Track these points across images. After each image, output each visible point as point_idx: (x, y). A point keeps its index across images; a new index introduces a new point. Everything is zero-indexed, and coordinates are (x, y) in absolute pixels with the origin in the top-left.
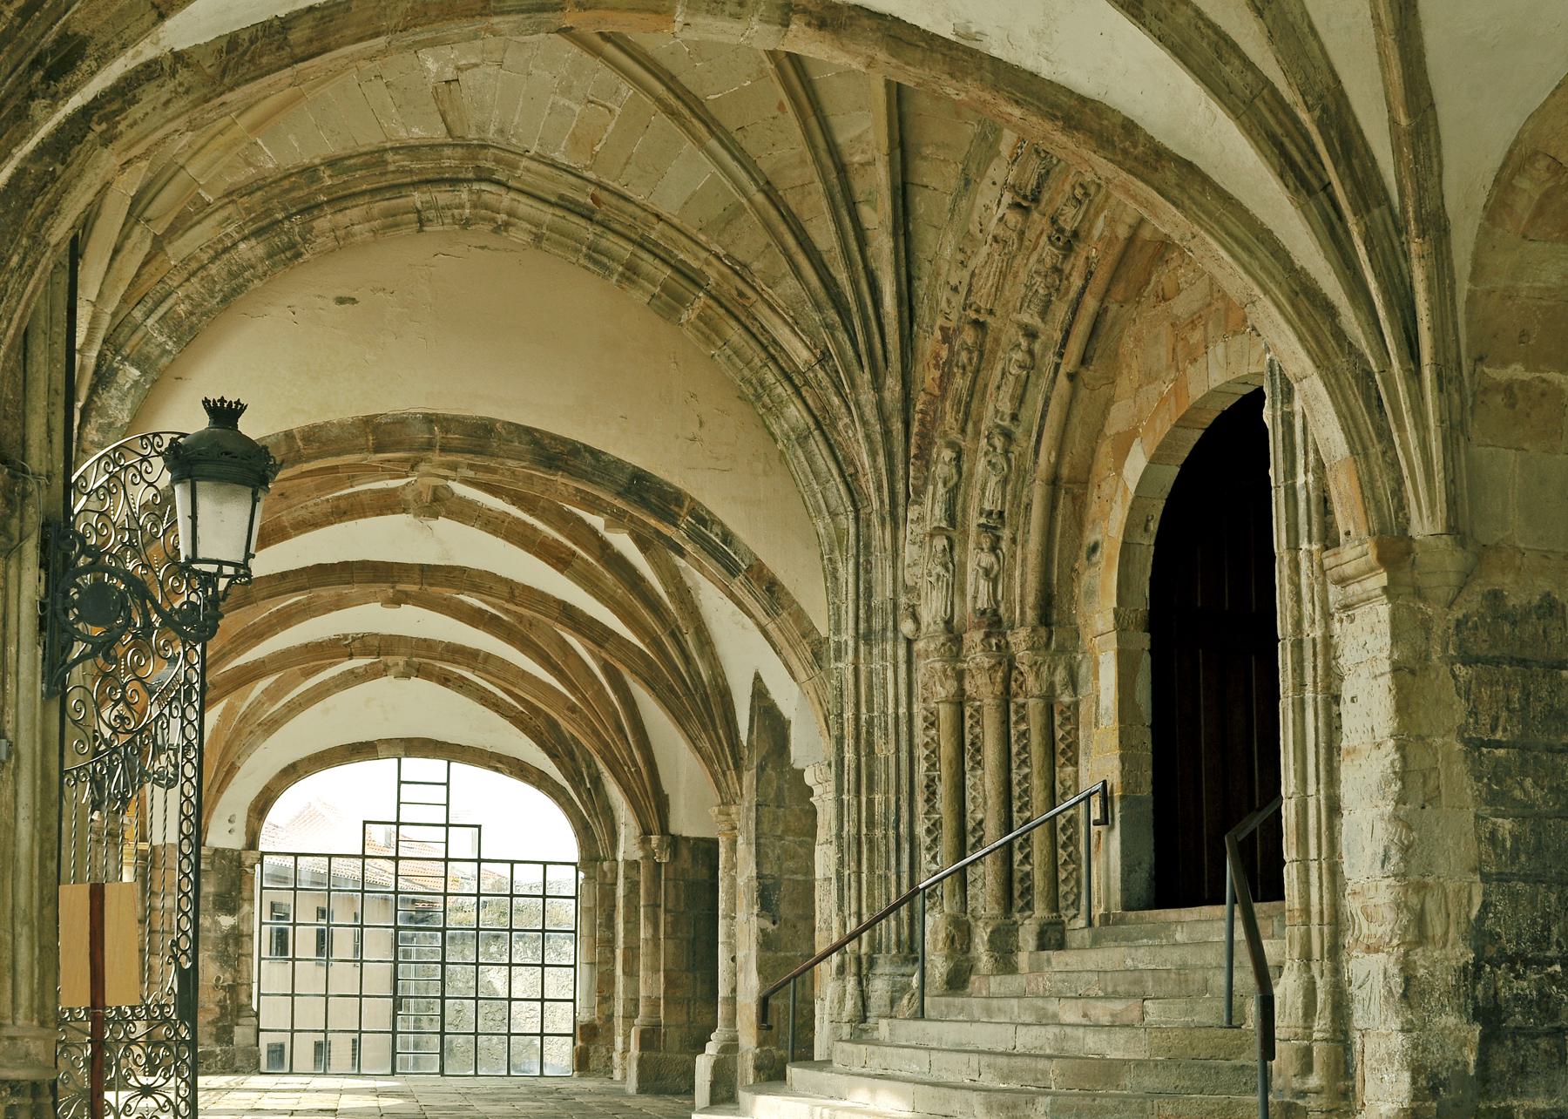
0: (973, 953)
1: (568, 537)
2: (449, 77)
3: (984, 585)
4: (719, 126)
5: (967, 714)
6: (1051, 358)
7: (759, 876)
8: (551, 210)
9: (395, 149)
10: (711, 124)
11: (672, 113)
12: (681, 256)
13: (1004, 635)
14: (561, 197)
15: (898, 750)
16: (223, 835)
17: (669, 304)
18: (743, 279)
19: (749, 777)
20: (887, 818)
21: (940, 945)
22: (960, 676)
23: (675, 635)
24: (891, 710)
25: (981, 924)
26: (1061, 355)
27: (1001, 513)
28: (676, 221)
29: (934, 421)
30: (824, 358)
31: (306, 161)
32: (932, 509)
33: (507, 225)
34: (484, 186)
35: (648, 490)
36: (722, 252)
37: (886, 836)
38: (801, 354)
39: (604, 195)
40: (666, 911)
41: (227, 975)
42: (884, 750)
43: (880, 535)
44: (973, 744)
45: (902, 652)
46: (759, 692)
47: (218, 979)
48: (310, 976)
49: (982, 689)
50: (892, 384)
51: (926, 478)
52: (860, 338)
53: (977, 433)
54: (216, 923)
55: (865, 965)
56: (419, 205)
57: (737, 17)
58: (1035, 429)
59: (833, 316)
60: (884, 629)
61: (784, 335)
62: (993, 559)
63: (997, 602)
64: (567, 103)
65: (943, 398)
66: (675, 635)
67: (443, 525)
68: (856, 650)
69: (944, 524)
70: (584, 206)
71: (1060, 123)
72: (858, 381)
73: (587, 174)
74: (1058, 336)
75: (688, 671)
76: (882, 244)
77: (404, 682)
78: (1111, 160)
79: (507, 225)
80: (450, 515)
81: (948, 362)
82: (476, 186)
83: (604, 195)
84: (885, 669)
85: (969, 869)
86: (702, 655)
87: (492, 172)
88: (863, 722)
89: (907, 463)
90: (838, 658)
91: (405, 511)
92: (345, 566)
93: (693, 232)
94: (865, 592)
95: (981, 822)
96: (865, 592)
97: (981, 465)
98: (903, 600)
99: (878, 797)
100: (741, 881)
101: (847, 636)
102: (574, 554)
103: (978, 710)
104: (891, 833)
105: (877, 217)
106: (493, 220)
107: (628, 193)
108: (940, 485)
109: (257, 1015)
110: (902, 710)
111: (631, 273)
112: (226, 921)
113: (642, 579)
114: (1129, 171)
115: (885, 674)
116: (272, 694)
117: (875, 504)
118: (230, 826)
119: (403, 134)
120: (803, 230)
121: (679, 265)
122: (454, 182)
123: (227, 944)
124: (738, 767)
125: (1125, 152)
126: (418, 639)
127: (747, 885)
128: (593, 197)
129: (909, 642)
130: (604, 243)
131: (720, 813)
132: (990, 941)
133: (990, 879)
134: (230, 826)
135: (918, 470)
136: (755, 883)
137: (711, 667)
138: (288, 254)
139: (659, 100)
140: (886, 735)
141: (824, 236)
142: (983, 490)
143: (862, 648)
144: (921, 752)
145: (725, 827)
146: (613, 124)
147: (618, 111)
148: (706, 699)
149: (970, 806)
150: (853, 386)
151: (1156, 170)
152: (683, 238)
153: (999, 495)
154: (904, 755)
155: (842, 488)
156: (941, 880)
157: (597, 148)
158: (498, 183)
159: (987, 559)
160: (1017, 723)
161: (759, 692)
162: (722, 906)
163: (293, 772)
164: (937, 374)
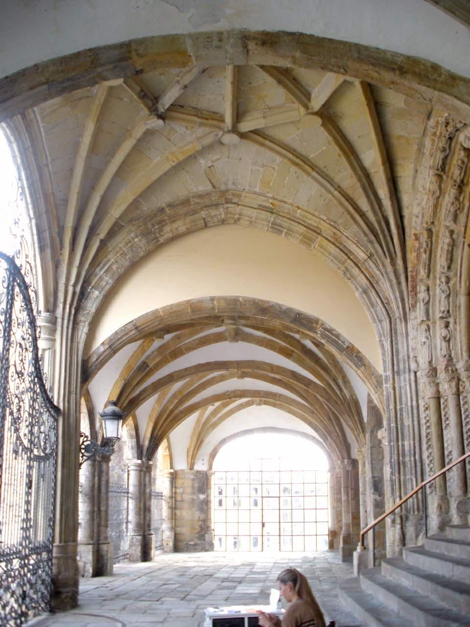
0: (450, 513)
1: (288, 344)
2: (209, 165)
3: (444, 344)
4: (316, 167)
5: (442, 402)
6: (461, 239)
7: (373, 477)
8: (256, 211)
9: (194, 197)
10: (313, 167)
11: (297, 165)
12: (309, 222)
13: (454, 365)
14: (260, 205)
15: (413, 421)
16: (201, 466)
17: (307, 241)
18: (335, 228)
19: (368, 436)
20: (410, 452)
21: (435, 510)
22: (437, 385)
23: (335, 380)
24: (409, 404)
25: (453, 500)
26: (465, 237)
27: (448, 311)
28: (305, 208)
29: (416, 275)
30: (370, 256)
31: (159, 205)
32: (419, 313)
33: (239, 219)
34: (229, 205)
35: (303, 319)
36: (325, 218)
37: (410, 461)
38: (361, 255)
39: (275, 202)
40: (351, 489)
41: (203, 516)
42: (407, 422)
43: (400, 327)
44: (445, 415)
45: (412, 377)
46: (370, 401)
47: (199, 517)
48: (232, 516)
49: (447, 391)
50: (400, 262)
51: (416, 300)
52: (384, 245)
53: (435, 277)
54: (198, 497)
55: (404, 519)
56: (204, 216)
57: (218, 47)
58: (459, 272)
59: (373, 238)
60: (404, 368)
61: (353, 248)
62: (447, 332)
63: (450, 351)
64: (257, 168)
65: (418, 264)
66: (335, 380)
67: (241, 344)
68: (394, 378)
69: (425, 319)
70: (268, 208)
71: (398, 72)
72: (386, 264)
73: (268, 195)
74: (463, 229)
75: (341, 394)
76: (387, 203)
77: (260, 407)
78: (429, 87)
79: (239, 219)
80: (243, 340)
81: (419, 248)
82: (225, 206)
83: (275, 202)
84: (406, 385)
85: (447, 474)
86: (346, 387)
87: (231, 199)
88: (398, 410)
89: (408, 297)
90: (386, 383)
91: (226, 340)
92: (208, 364)
93: (312, 212)
94: (394, 352)
95: (451, 452)
96: (394, 352)
97: (438, 291)
98: (411, 355)
99: (406, 443)
100: (367, 479)
101: (389, 373)
102: (293, 351)
103: (446, 400)
104: (412, 459)
105: (383, 192)
106: (234, 218)
107: (285, 200)
108: (422, 302)
109: (214, 530)
110: (414, 403)
111: (290, 232)
112: (202, 497)
113: (320, 359)
114: (440, 90)
115: (406, 388)
116: (215, 413)
117: (397, 313)
118: (203, 462)
119: (195, 190)
120: (356, 204)
121: (308, 226)
122: (217, 205)
123: (202, 505)
124: (364, 432)
125: (435, 80)
126: (254, 391)
127: (369, 480)
128: (272, 204)
129: (415, 373)
130: (278, 221)
131: (358, 451)
132: (458, 508)
133: (456, 478)
134: (203, 462)
135: (413, 297)
136: (371, 480)
137: (350, 392)
138: (155, 241)
139: (290, 160)
140: (408, 415)
141: (364, 205)
142: (440, 302)
143: (396, 377)
144: (423, 421)
145: (361, 457)
146: (276, 174)
147: (277, 168)
148: (349, 406)
149: (446, 445)
150: (384, 265)
151: (453, 86)
152: (309, 215)
153: (446, 302)
154: (416, 423)
155: (383, 309)
156: (434, 479)
157: (271, 184)
158: (234, 203)
159: (444, 332)
160: (464, 405)
161: (370, 401)
162: (361, 489)
163: (223, 441)
164: (415, 254)
